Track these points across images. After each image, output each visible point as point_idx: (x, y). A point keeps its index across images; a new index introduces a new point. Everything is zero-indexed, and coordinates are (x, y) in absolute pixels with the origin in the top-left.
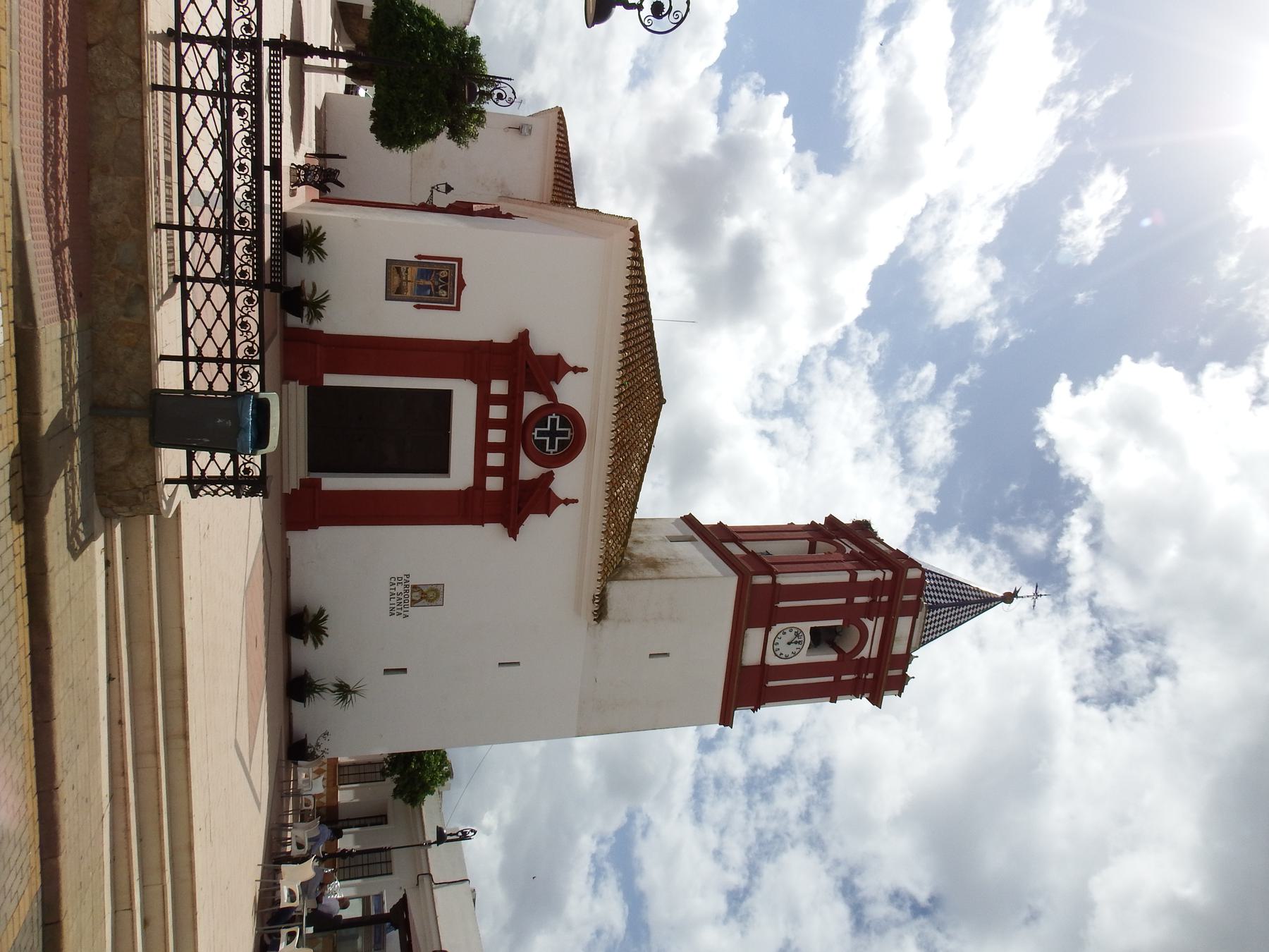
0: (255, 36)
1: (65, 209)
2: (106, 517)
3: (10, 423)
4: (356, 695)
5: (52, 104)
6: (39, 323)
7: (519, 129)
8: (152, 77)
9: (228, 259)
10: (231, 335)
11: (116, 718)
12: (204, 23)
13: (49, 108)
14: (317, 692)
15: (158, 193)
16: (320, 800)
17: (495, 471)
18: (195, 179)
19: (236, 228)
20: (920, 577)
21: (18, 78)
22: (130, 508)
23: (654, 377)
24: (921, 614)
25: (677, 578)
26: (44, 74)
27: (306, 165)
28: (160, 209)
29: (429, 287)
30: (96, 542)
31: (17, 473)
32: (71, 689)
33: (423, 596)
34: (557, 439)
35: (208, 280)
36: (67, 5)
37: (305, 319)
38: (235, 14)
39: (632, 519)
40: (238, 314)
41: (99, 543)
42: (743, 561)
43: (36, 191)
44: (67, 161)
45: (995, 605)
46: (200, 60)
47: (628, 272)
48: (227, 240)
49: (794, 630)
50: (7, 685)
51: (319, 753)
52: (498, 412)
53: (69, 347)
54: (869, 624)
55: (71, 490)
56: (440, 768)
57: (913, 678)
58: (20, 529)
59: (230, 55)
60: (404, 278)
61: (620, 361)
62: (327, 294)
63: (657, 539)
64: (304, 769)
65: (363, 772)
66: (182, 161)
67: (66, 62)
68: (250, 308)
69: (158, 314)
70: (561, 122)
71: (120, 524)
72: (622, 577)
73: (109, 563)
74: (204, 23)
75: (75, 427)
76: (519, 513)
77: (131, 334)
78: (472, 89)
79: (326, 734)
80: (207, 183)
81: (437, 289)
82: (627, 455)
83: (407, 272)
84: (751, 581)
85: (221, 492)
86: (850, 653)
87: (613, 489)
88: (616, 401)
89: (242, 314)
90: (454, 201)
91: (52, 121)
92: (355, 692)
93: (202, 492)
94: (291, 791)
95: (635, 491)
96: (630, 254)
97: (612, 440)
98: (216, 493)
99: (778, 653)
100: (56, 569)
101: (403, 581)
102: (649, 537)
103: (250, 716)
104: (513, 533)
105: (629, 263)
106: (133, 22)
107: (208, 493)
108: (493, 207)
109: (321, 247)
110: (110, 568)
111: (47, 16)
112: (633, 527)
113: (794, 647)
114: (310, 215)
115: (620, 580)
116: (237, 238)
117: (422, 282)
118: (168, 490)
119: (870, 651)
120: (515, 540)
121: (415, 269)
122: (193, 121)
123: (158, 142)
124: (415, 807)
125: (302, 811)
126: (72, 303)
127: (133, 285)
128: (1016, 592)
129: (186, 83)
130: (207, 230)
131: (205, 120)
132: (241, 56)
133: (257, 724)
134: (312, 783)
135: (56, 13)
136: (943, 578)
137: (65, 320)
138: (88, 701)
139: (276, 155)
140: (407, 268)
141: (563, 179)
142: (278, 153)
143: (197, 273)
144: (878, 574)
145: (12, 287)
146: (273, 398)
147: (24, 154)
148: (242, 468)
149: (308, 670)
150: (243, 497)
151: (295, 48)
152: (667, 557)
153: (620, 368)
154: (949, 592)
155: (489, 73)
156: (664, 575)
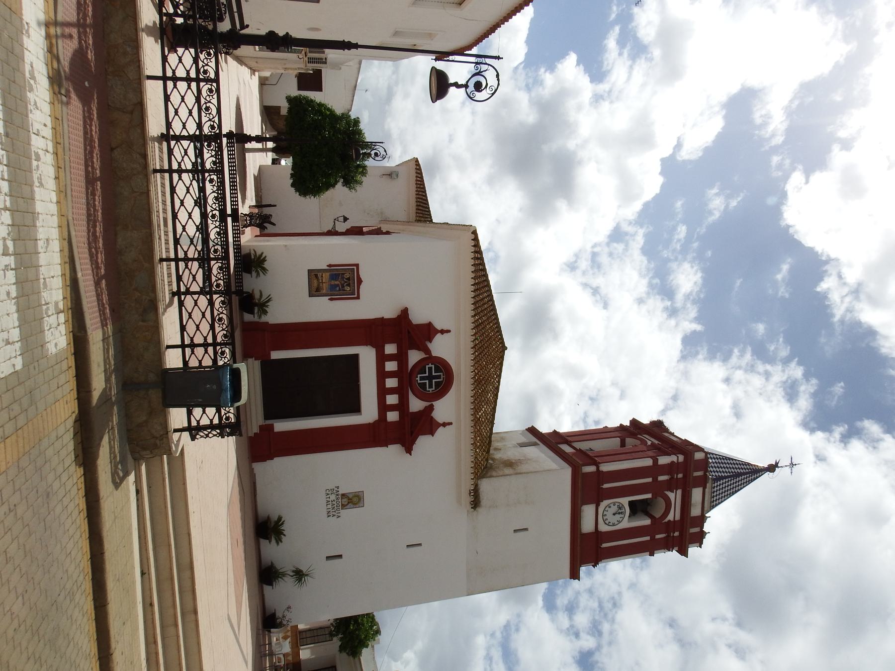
0: (218, 132)
1: (101, 255)
2: (135, 459)
3: (73, 399)
4: (309, 578)
5: (91, 188)
6: (88, 330)
7: (390, 175)
8: (153, 165)
9: (207, 277)
10: (212, 327)
11: (148, 602)
12: (184, 127)
13: (90, 191)
14: (281, 578)
15: (160, 238)
16: (288, 658)
17: (392, 408)
18: (184, 228)
19: (212, 256)
20: (704, 458)
21: (69, 173)
22: (151, 452)
23: (497, 332)
24: (709, 485)
25: (528, 473)
26: (85, 170)
27: (250, 213)
28: (162, 248)
29: (338, 285)
30: (130, 477)
31: (78, 432)
32: (118, 582)
33: (350, 501)
34: (434, 381)
35: (195, 293)
36: (97, 125)
37: (256, 316)
38: (204, 119)
39: (491, 433)
40: (216, 313)
41: (132, 478)
42: (574, 457)
43: (83, 245)
44: (102, 224)
45: (762, 475)
46: (183, 152)
47: (472, 262)
48: (205, 249)
49: (617, 504)
50: (76, 581)
51: (285, 622)
52: (391, 366)
53: (108, 345)
54: (671, 495)
55: (112, 442)
56: (371, 627)
57: (709, 533)
58: (81, 471)
59: (202, 146)
60: (321, 281)
61: (473, 323)
62: (270, 297)
63: (511, 446)
64: (275, 634)
65: (316, 635)
66: (175, 216)
67: (99, 161)
68: (209, 60)
69: (164, 317)
70: (418, 167)
71: (144, 464)
72: (489, 475)
73: (138, 492)
74: (184, 127)
75: (113, 399)
76: (411, 435)
77: (147, 333)
78: (358, 152)
79: (289, 607)
80: (191, 230)
81: (343, 286)
82: (483, 388)
83: (322, 277)
84: (581, 471)
85: (210, 435)
86: (659, 518)
87: (476, 413)
88: (472, 351)
89: (219, 313)
90: (350, 227)
91: (91, 199)
92: (307, 575)
93: (198, 436)
94: (267, 652)
95: (491, 413)
96: (473, 249)
97: (472, 378)
98: (207, 436)
99: (607, 522)
100: (105, 497)
101: (335, 491)
102: (505, 445)
103: (237, 597)
104: (409, 450)
105: (472, 255)
106: (139, 131)
107: (202, 437)
108: (376, 228)
109: (264, 266)
110: (139, 495)
111: (85, 133)
112: (493, 439)
113: (618, 517)
114: (257, 246)
115: (487, 477)
116: (213, 263)
117: (333, 282)
118: (176, 436)
119: (674, 515)
120: (411, 455)
121: (328, 274)
122: (181, 190)
123: (159, 205)
124: (356, 659)
125: (275, 667)
126: (109, 316)
127: (147, 300)
128: (777, 464)
129: (175, 166)
130: (193, 260)
131: (188, 189)
132: (209, 146)
133: (242, 601)
134: (281, 645)
135: (91, 130)
136: (721, 457)
137: (105, 328)
138: (129, 590)
139: (236, 224)
140: (322, 274)
141: (422, 204)
142: (235, 226)
143: (188, 289)
144: (673, 458)
145: (71, 308)
146: (242, 367)
147: (75, 222)
148: (224, 417)
149: (273, 561)
150: (226, 437)
151: (239, 138)
152: (519, 458)
153: (473, 327)
154: (727, 467)
155: (367, 140)
156: (519, 471)
